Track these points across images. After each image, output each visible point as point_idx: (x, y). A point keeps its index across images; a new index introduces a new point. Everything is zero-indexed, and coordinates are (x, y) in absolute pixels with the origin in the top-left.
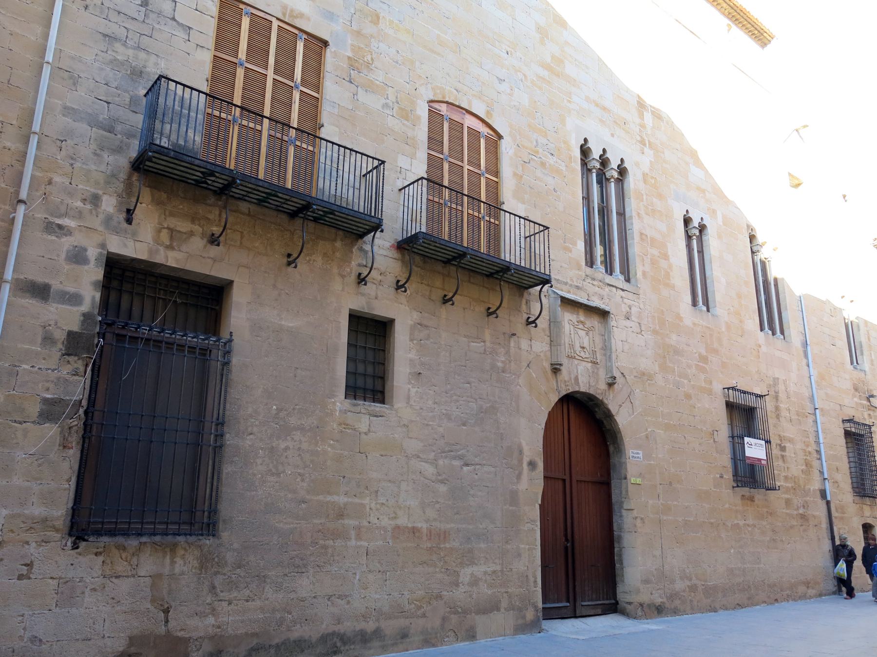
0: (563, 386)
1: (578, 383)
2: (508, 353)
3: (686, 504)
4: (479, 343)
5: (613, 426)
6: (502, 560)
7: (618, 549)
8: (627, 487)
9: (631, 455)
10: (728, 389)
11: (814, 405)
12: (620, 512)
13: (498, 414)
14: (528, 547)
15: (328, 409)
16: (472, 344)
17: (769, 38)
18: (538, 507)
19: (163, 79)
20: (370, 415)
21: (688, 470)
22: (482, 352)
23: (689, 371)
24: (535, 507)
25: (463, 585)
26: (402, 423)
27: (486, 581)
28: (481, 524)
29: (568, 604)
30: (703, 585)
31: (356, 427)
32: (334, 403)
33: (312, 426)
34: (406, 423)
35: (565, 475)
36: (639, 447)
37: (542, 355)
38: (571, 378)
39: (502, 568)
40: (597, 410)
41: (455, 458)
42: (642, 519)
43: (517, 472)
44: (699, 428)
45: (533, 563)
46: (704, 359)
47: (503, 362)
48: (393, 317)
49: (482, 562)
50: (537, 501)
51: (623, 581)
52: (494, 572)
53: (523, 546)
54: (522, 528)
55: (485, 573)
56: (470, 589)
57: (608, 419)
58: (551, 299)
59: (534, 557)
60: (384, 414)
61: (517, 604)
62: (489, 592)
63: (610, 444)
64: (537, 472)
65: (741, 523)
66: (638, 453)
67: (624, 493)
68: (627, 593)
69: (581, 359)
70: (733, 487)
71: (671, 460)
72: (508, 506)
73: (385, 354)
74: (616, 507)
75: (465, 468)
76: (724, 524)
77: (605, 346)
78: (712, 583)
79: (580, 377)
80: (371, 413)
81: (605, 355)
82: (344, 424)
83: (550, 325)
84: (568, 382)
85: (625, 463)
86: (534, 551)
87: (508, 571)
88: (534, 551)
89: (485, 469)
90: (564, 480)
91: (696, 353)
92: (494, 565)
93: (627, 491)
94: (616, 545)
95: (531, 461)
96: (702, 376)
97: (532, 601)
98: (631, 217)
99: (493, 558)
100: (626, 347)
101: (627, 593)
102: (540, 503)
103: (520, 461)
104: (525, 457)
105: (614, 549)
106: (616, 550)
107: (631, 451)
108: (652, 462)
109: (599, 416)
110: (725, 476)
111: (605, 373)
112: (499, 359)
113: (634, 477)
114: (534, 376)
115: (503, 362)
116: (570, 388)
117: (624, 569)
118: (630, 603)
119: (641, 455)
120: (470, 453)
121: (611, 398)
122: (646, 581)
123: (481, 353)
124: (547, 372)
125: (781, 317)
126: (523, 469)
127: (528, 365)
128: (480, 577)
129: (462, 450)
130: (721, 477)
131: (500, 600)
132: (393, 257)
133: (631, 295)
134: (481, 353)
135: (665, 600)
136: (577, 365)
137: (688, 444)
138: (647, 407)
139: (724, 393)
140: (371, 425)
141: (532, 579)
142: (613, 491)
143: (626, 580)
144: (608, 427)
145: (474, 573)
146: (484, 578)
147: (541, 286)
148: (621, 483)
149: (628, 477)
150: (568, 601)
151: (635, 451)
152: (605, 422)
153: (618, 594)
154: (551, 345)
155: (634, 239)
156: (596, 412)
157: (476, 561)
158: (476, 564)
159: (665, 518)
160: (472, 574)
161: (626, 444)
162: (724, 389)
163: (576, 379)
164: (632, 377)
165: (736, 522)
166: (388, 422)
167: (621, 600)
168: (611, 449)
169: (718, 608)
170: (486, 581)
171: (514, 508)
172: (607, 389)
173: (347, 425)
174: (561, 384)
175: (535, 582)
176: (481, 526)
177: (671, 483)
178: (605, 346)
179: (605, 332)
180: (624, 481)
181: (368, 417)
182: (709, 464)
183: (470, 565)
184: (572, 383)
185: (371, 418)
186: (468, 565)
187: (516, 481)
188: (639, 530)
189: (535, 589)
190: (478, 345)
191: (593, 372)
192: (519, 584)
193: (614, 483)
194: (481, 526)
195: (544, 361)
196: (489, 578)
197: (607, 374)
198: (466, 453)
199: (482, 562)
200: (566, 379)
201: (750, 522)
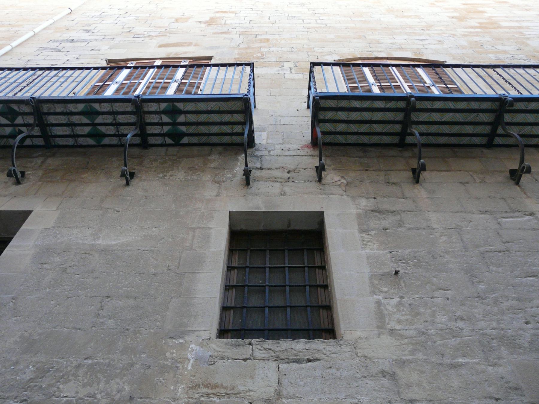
4: (521, 217)
15: (166, 359)
19: (282, 143)
20: (277, 359)
22: (281, 142)
26: (374, 369)
31: (241, 388)
32: (183, 347)
33: (118, 396)
34: (387, 367)
48: (318, 209)
60: (317, 356)
80: (284, 355)
82: (206, 386)
125: (193, 146)
132: (308, 154)
140: (285, 382)
147: (173, 143)
166: (332, 371)
173: (215, 387)
181: (275, 364)
185: (282, 366)
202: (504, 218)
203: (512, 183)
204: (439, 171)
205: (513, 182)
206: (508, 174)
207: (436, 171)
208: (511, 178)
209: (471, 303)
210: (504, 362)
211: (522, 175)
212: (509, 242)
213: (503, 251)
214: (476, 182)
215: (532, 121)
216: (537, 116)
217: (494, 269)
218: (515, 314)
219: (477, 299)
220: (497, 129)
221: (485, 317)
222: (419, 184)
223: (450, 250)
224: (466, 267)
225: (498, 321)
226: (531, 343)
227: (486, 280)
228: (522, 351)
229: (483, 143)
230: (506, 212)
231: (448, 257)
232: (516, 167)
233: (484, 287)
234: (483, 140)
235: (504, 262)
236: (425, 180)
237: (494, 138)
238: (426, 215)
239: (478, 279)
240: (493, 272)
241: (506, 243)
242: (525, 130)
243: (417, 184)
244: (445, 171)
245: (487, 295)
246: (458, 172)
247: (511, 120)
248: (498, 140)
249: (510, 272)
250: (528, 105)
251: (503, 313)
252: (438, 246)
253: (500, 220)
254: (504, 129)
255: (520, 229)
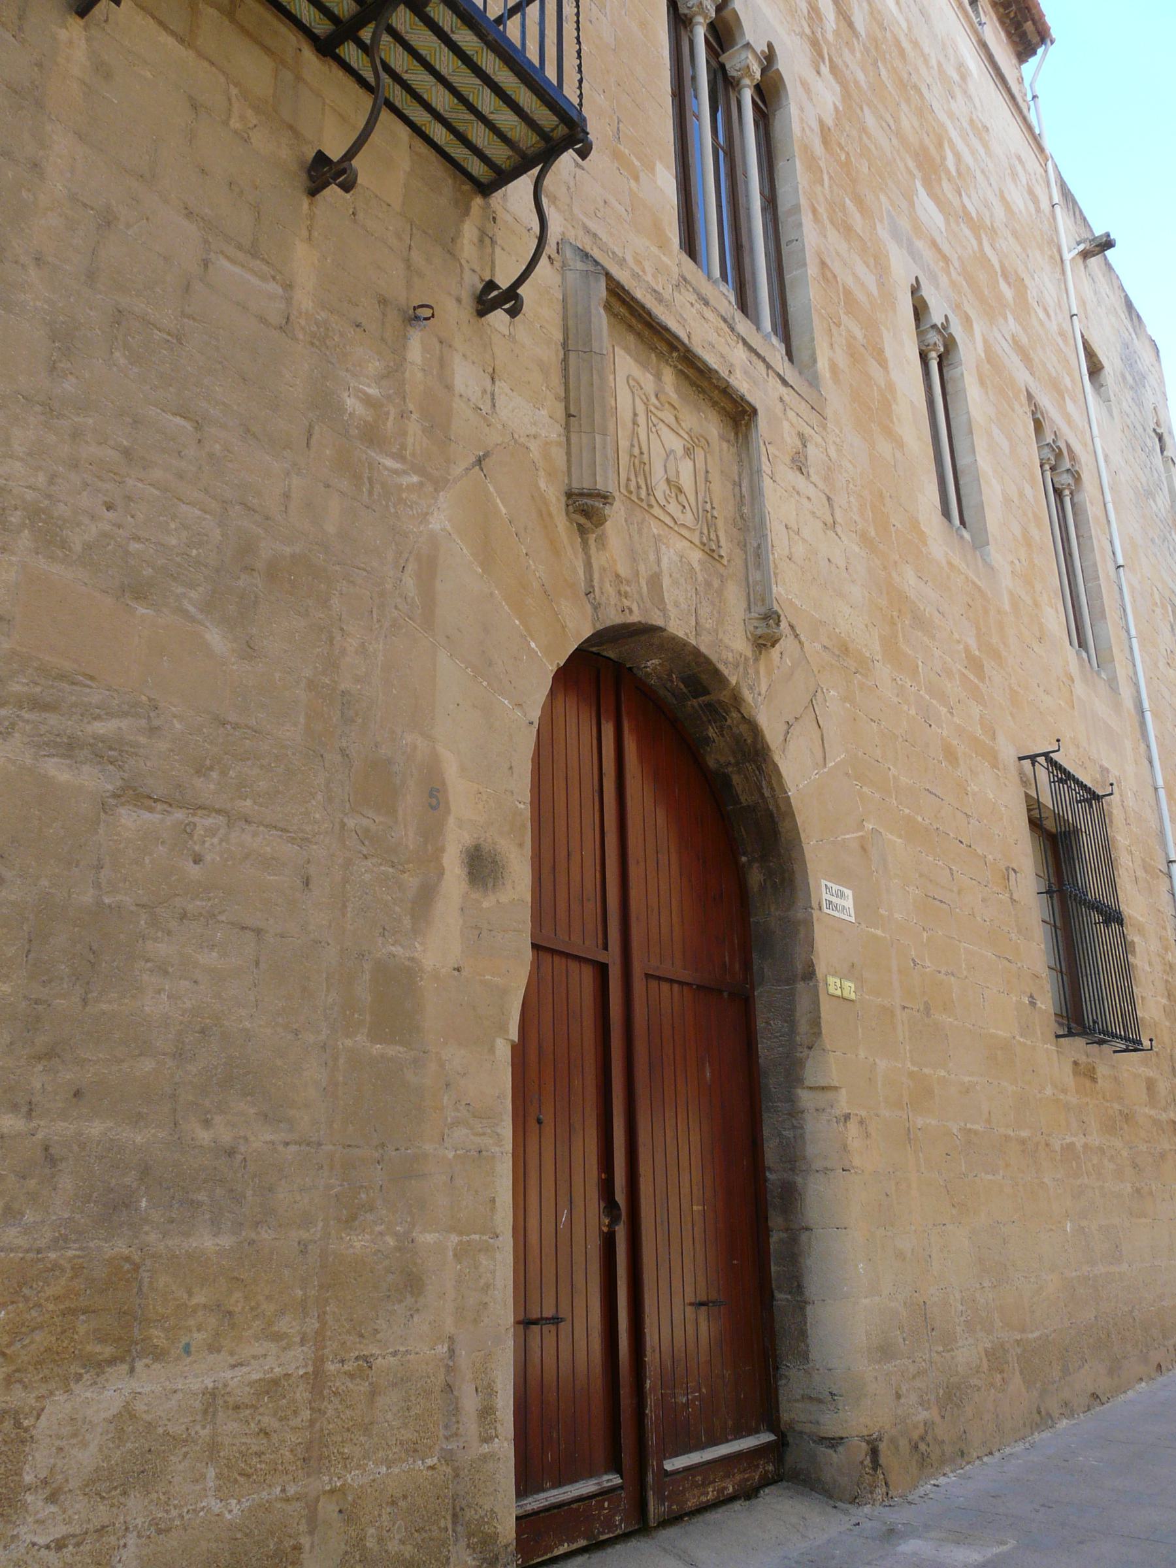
0: (610, 590)
1: (662, 600)
2: (394, 372)
3: (967, 1079)
4: (263, 278)
5: (767, 793)
6: (321, 1317)
7: (784, 1235)
8: (816, 1003)
9: (825, 896)
10: (1033, 758)
11: (1167, 854)
12: (791, 1099)
13: (335, 602)
14: (454, 1238)
16: (226, 264)
17: (1035, 39)
18: (503, 1052)
21: (965, 973)
23: (949, 685)
24: (492, 1050)
25: (52, 1498)
27: (213, 1448)
28: (207, 1123)
29: (615, 1480)
30: (1018, 1342)
35: (606, 948)
36: (842, 876)
37: (533, 446)
38: (637, 573)
39: (319, 1361)
40: (711, 732)
41: (69, 748)
42: (861, 1122)
43: (412, 882)
44: (980, 852)
45: (475, 1321)
46: (975, 665)
47: (368, 401)
49: (199, 1337)
50: (502, 1028)
51: (805, 1356)
52: (272, 1386)
53: (430, 1238)
54: (429, 1148)
55: (213, 1399)
56: (102, 1515)
57: (751, 767)
58: (570, 275)
59: (487, 1288)
61: (393, 1546)
62: (233, 1511)
63: (750, 862)
64: (504, 899)
65: (1079, 1142)
66: (842, 896)
67: (803, 1027)
68: (820, 1401)
69: (671, 524)
70: (1058, 1036)
71: (925, 934)
72: (361, 1038)
73: (626, 1537)
74: (772, 1083)
75: (130, 819)
76: (1047, 1145)
77: (742, 517)
78: (1036, 1334)
79: (666, 582)
81: (743, 546)
83: (565, 360)
84: (628, 583)
85: (809, 923)
86: (484, 1260)
87: (351, 1376)
88: (484, 1260)
89: (66, 385)
90: (602, 970)
91: (958, 642)
92: (272, 1347)
93: (816, 1022)
94: (775, 1220)
95: (477, 848)
96: (976, 710)
97: (469, 1514)
98: (797, 208)
99: (269, 1308)
100: (799, 550)
101: (820, 1401)
102: (514, 1035)
103: (432, 833)
104: (451, 821)
105: (768, 1236)
106: (775, 1238)
107: (824, 882)
108: (879, 932)
109: (717, 756)
110: (1039, 1004)
111: (744, 605)
112: (353, 383)
113: (835, 975)
114: (504, 511)
115: (368, 401)
116: (635, 608)
117: (809, 1308)
118: (834, 1442)
119: (849, 903)
120: (163, 746)
121: (763, 692)
122: (884, 1352)
123: (263, 320)
124: (550, 515)
126: (441, 873)
127: (479, 461)
128: (176, 1429)
129: (111, 715)
130: (1033, 1004)
131: (297, 1548)
133: (803, 408)
134: (263, 320)
135: (933, 1414)
136: (657, 540)
137: (959, 892)
138: (860, 754)
139: (1022, 774)
141: (470, 1403)
142: (760, 1024)
143: (814, 1354)
144: (745, 799)
145: (140, 1406)
146: (205, 1433)
148: (792, 994)
149: (821, 969)
150: (619, 1470)
151: (835, 887)
152: (736, 779)
153: (783, 1405)
154: (567, 428)
155: (805, 265)
156: (707, 740)
157: (158, 1336)
158: (159, 1355)
159: (920, 1122)
160: (128, 1413)
161: (808, 855)
162: (1020, 759)
163: (655, 582)
164: (819, 647)
165: (1068, 1140)
167: (798, 1427)
168: (755, 877)
169: (1056, 1415)
170: (213, 1448)
171: (392, 1051)
172: (749, 654)
174: (601, 581)
175: (487, 1412)
176: (204, 1136)
177: (927, 1010)
178: (742, 517)
179: (740, 475)
180: (801, 986)
182: (1008, 964)
183: (112, 1361)
184: (640, 593)
186: (100, 1366)
187: (407, 921)
188: (857, 1161)
189: (485, 1448)
190: (255, 281)
191: (708, 584)
192: (408, 1435)
193: (763, 996)
194: (204, 1136)
195: (542, 473)
196: (233, 1426)
197: (749, 609)
198: (142, 740)
199: (199, 1337)
200: (623, 570)
201: (1095, 1139)
202: (227, 258)
203: (302, 179)
204: (161, 23)
205: (309, 184)
206: (311, 154)
207: (154, 17)
208: (309, 171)
209: (18, 411)
210: (9, 560)
211: (330, 184)
212: (194, 319)
213: (169, 334)
214: (228, 124)
215: (444, 71)
216: (458, 68)
217: (122, 361)
218: (98, 477)
219: (38, 408)
220: (364, 25)
221: (30, 454)
222: (81, 22)
223: (50, 259)
224: (63, 323)
225: (52, 479)
226: (88, 547)
227: (87, 376)
228: (61, 555)
229: (316, 31)
230: (240, 247)
231: (33, 273)
232: (335, 154)
233: (73, 390)
234: (322, 27)
235: (153, 359)
236: (106, 21)
237: (346, 40)
238: (49, 128)
239: (1131, 864)
240: (115, 369)
241: (188, 318)
242: (420, 77)
243: (78, 19)
244: (173, 33)
245: (66, 412)
246: (206, 64)
247: (407, 32)
248: (350, 52)
249: (149, 387)
250: (459, 29)
251: (75, 465)
252: (27, 231)
253: (212, 256)
254: (375, 37)
255: (238, 304)
